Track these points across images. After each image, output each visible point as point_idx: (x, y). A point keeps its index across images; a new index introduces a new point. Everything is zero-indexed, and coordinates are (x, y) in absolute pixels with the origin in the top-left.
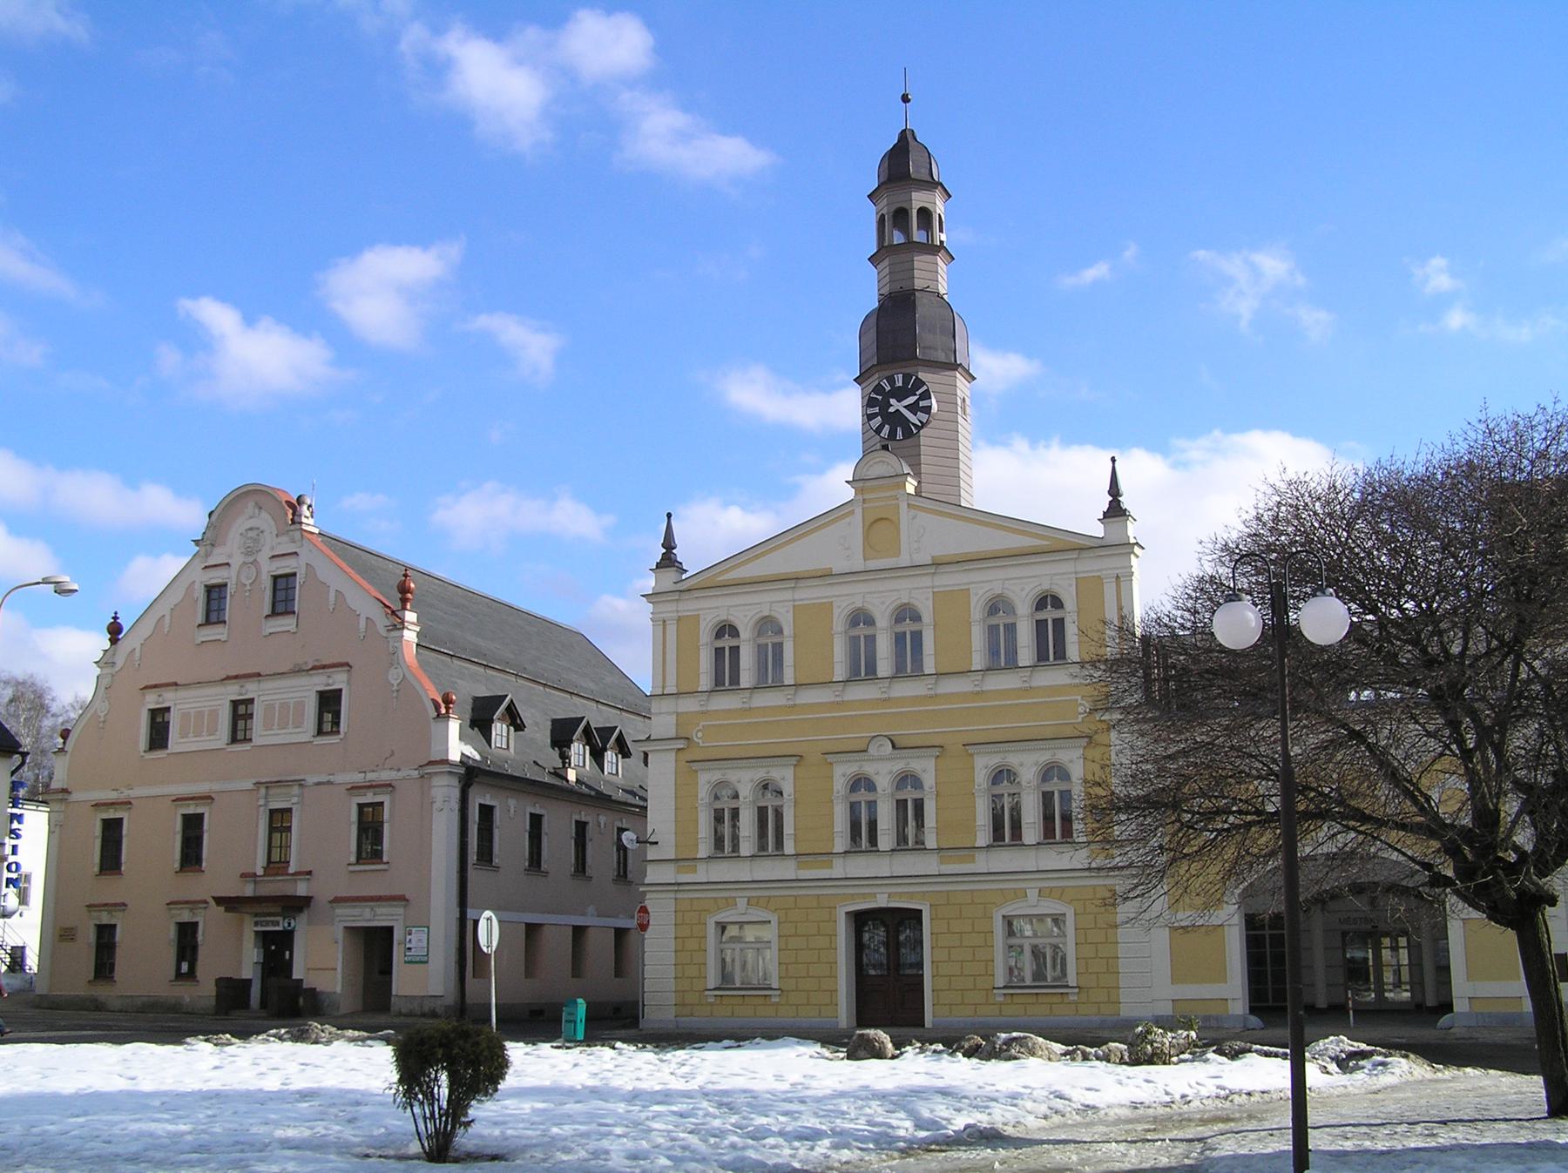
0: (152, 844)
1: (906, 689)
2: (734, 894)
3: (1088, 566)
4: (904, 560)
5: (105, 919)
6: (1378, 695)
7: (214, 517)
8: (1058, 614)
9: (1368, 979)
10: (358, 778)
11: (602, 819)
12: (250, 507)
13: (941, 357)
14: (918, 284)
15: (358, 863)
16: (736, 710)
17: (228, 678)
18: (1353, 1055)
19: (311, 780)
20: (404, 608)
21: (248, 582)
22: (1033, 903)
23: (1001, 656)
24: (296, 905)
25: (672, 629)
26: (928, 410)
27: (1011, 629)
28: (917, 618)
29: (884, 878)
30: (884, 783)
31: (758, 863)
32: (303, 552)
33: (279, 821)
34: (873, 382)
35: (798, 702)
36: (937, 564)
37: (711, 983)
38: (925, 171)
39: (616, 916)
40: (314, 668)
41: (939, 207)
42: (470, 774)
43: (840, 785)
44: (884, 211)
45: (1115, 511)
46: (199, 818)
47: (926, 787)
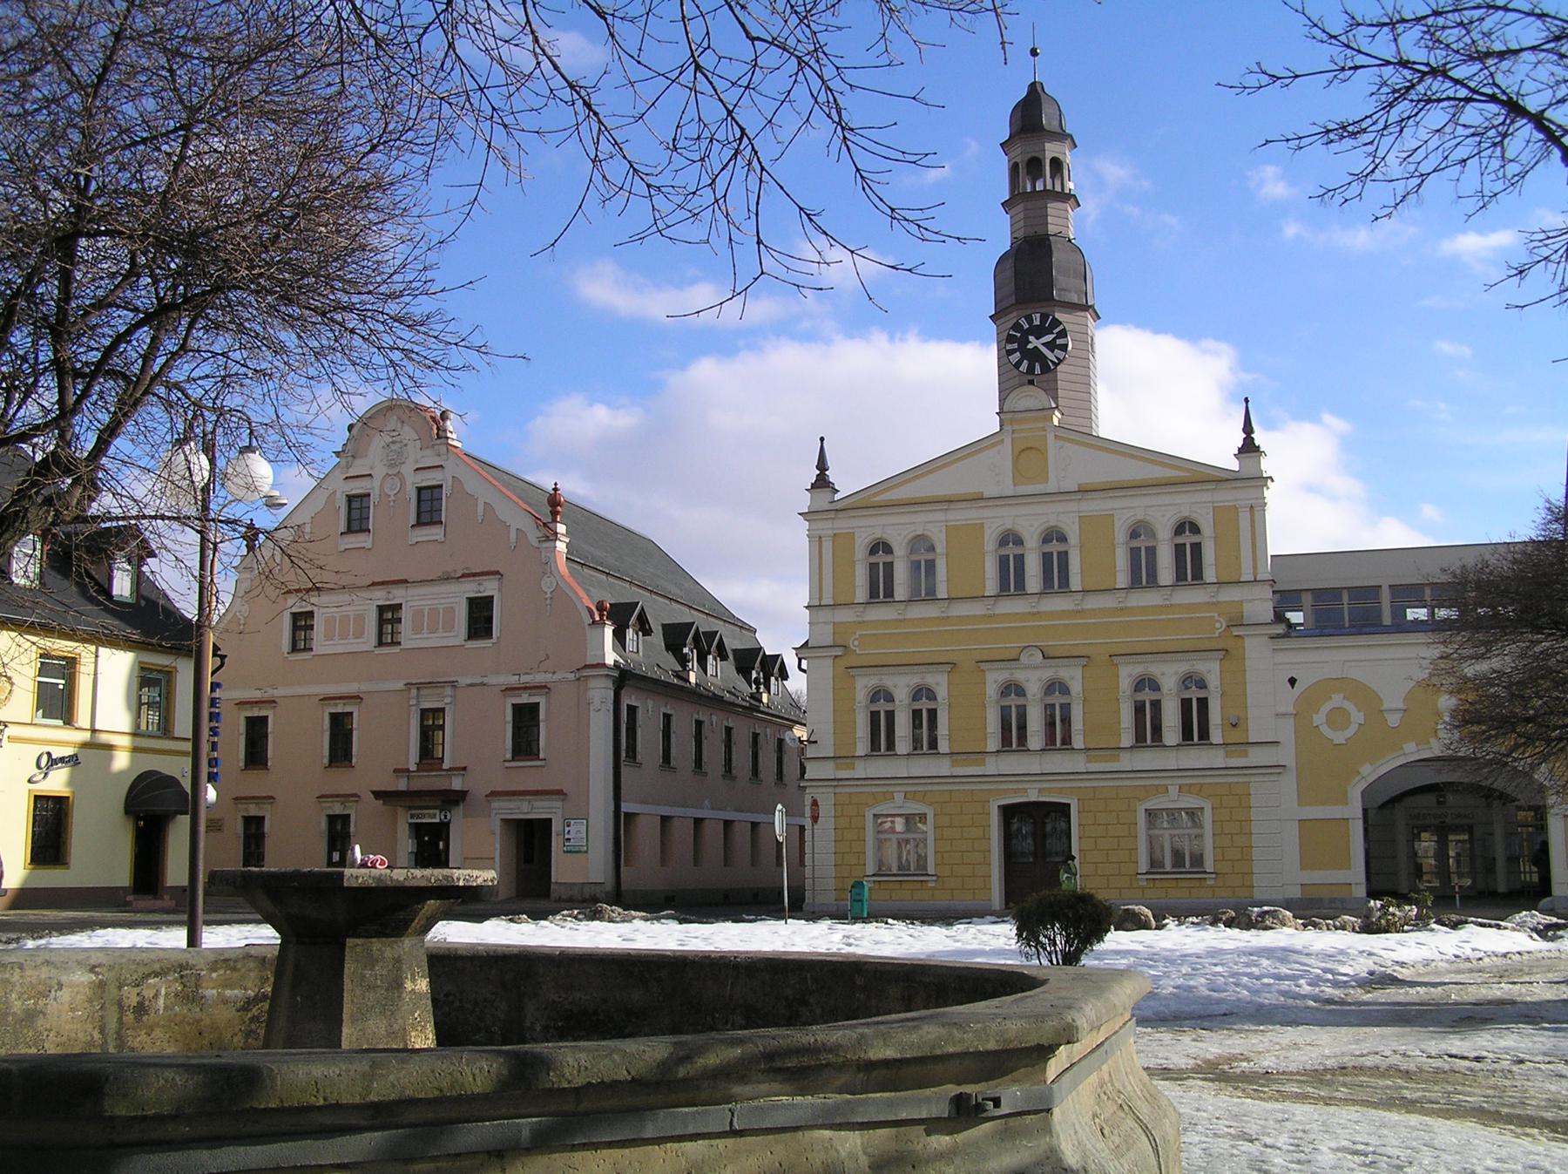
0: (298, 742)
1: (1190, 596)
2: (891, 789)
3: (1225, 496)
4: (1052, 486)
5: (253, 811)
6: (1432, 614)
7: (355, 431)
8: (1195, 539)
10: (513, 680)
11: (714, 718)
13: (1074, 298)
14: (1052, 229)
15: (513, 759)
16: (1024, 614)
17: (374, 584)
18: (1549, 927)
19: (463, 681)
20: (555, 521)
21: (392, 493)
22: (1173, 799)
23: (1142, 573)
24: (453, 799)
25: (828, 545)
26: (1064, 348)
27: (1151, 552)
28: (1063, 539)
29: (1034, 774)
30: (1034, 688)
31: (914, 760)
32: (448, 465)
33: (430, 725)
34: (1011, 319)
35: (997, 612)
36: (1084, 491)
37: (870, 871)
38: (1055, 123)
39: (724, 809)
40: (463, 576)
41: (1069, 158)
42: (623, 678)
43: (992, 690)
44: (1018, 160)
45: (1249, 448)
46: (263, 720)
47: (1029, 696)
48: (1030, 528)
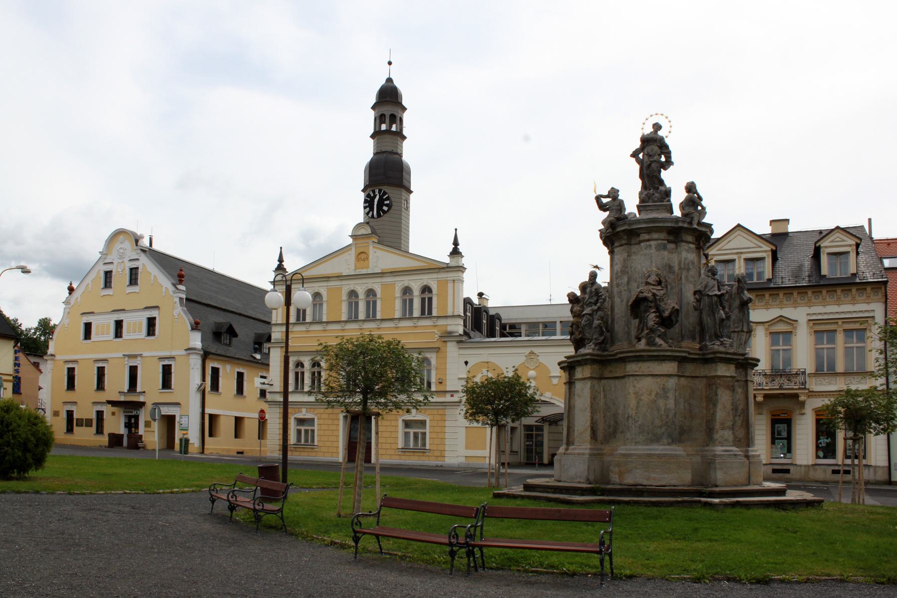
0: (86, 378)
9: (825, 457)
12: (121, 237)
17: (146, 308)
33: (133, 371)
45: (455, 252)
48: (361, 288)
